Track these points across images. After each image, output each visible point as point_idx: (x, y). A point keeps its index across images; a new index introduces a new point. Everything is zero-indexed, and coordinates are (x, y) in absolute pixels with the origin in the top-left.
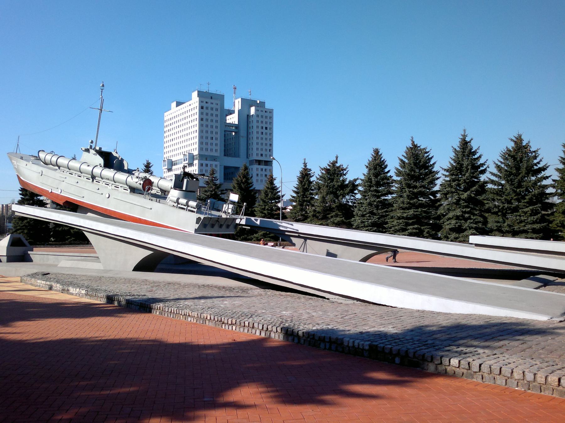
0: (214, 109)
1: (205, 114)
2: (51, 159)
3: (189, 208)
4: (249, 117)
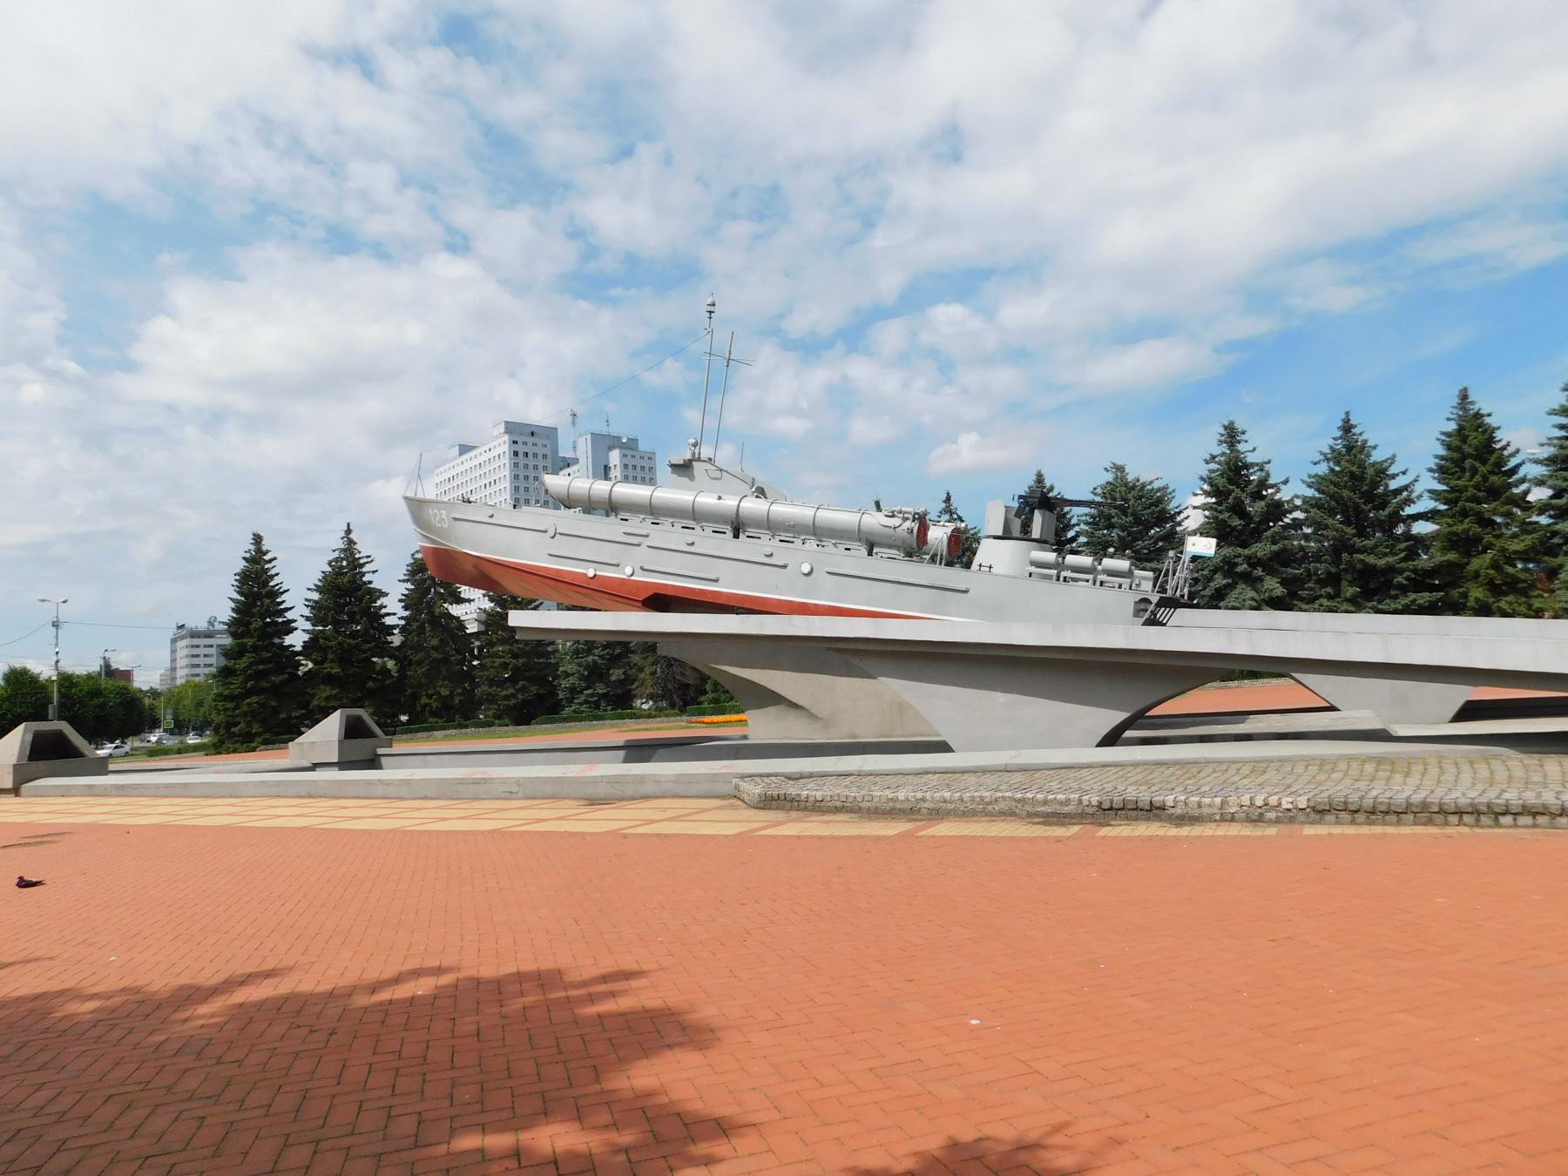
1: (521, 466)
3: (1064, 574)
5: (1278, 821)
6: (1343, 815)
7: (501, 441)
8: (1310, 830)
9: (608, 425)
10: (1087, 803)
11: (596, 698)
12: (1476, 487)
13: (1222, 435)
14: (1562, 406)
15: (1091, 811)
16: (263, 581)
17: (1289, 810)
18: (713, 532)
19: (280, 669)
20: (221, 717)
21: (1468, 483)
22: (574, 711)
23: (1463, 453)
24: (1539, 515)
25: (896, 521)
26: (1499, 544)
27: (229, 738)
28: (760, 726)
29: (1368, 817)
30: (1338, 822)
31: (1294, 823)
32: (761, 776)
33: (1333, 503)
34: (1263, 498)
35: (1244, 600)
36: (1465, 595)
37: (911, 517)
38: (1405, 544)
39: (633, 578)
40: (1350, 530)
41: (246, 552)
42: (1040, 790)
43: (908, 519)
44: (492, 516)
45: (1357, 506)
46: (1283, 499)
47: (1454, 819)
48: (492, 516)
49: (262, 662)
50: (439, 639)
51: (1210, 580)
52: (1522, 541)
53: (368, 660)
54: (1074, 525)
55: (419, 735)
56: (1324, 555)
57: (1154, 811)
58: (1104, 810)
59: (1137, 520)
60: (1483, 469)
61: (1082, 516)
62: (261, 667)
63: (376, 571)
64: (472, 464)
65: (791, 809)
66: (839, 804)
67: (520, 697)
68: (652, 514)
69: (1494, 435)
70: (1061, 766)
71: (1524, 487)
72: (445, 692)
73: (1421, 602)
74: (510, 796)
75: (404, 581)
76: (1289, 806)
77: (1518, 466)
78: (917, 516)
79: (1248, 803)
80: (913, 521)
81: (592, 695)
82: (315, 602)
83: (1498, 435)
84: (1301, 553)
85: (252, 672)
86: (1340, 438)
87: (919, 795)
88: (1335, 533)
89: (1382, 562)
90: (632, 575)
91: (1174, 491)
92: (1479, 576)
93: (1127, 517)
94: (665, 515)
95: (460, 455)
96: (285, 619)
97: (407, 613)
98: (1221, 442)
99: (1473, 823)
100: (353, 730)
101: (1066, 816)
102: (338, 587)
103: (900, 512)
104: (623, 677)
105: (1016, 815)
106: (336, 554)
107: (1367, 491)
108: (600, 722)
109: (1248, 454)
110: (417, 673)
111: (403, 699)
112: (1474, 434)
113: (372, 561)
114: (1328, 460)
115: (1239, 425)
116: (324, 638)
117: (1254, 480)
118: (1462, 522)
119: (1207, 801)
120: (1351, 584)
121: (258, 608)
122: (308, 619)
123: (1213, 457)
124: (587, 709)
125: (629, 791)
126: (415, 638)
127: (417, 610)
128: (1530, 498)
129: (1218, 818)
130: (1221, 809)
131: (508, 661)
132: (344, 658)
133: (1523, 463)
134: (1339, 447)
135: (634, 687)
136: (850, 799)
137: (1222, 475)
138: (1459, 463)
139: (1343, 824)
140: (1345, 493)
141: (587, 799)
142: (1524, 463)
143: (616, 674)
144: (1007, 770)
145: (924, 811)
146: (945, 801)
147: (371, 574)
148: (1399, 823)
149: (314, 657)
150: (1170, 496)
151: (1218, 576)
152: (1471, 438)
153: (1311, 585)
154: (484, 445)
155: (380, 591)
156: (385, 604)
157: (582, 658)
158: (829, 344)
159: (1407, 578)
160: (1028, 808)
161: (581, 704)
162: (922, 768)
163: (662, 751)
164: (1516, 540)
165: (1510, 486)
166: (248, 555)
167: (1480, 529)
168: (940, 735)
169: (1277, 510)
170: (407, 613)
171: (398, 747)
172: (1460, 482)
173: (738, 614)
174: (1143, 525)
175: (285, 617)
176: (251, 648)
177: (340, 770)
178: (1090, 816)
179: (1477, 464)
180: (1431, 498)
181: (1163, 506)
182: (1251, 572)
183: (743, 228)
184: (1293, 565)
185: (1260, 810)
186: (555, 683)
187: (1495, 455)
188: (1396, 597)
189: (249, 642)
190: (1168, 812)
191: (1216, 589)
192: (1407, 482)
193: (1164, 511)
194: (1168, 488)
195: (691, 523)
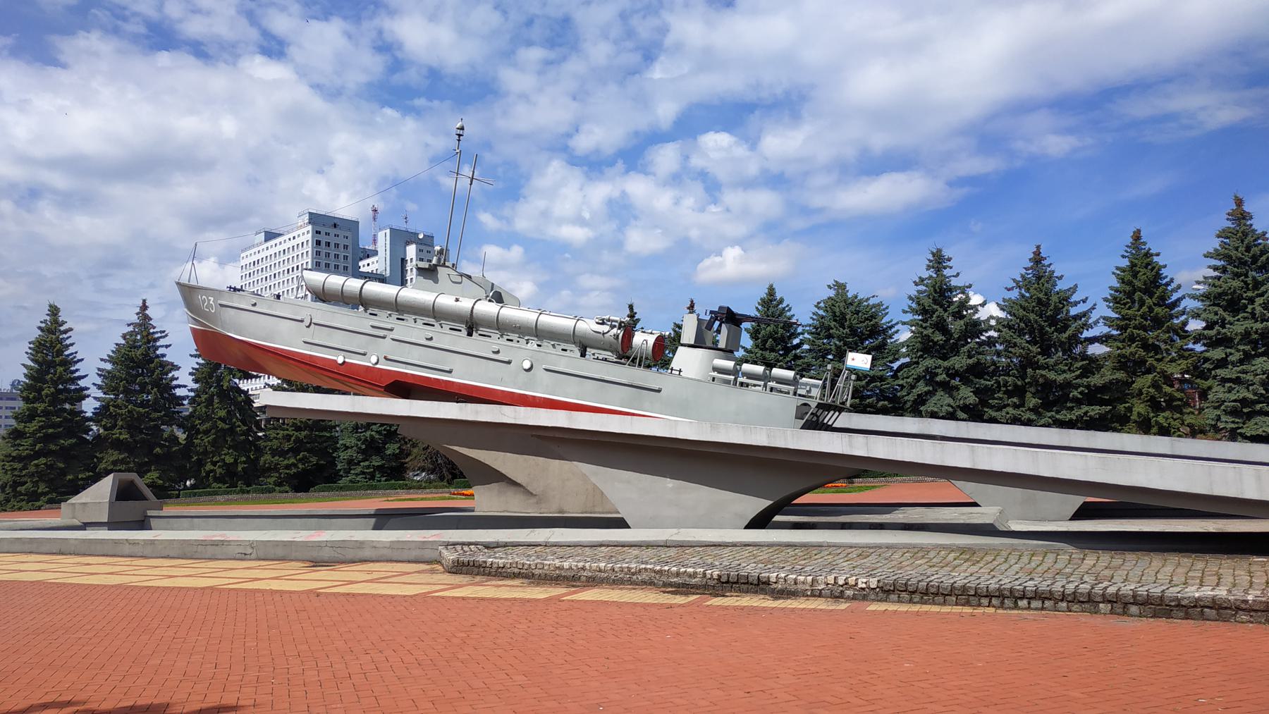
0: (341, 247)
1: (323, 254)
3: (741, 379)
5: (854, 598)
6: (904, 595)
7: (305, 230)
8: (874, 607)
9: (406, 222)
10: (710, 576)
11: (372, 470)
12: (1143, 317)
13: (930, 261)
14: (1216, 250)
15: (711, 583)
16: (58, 350)
17: (863, 589)
18: (451, 329)
19: (70, 433)
20: (7, 477)
21: (1136, 313)
22: (351, 481)
23: (1133, 286)
24: (1194, 343)
25: (605, 328)
26: (1160, 366)
27: (15, 497)
28: (485, 500)
29: (922, 598)
30: (900, 601)
31: (867, 600)
32: (463, 544)
33: (1022, 325)
34: (962, 317)
35: (942, 406)
36: (1130, 409)
37: (617, 324)
38: (1081, 364)
39: (378, 366)
40: (1035, 349)
41: (41, 322)
42: (792, 571)
43: (615, 326)
44: (254, 305)
45: (1042, 328)
46: (982, 319)
47: (985, 601)
48: (254, 305)
49: (53, 426)
50: (226, 410)
51: (913, 387)
52: (1179, 365)
53: (157, 427)
54: (799, 334)
55: (202, 499)
56: (1012, 369)
57: (760, 586)
58: (723, 583)
59: (853, 332)
60: (1149, 301)
61: (806, 326)
62: (51, 431)
63: (170, 345)
64: (276, 250)
65: (478, 574)
66: (516, 570)
67: (300, 466)
68: (397, 311)
69: (1161, 272)
70: (707, 544)
71: (1183, 318)
72: (229, 460)
73: (1092, 413)
74: (244, 557)
75: (195, 356)
76: (864, 586)
77: (1179, 300)
78: (623, 325)
79: (833, 582)
80: (619, 328)
81: (368, 467)
82: (109, 372)
83: (1164, 272)
84: (993, 367)
85: (42, 435)
86: (1031, 268)
87: (580, 565)
88: (1022, 351)
89: (1060, 378)
90: (377, 363)
91: (887, 308)
92: (1142, 394)
93: (844, 329)
94: (408, 313)
95: (266, 240)
96: (78, 387)
97: (196, 386)
98: (929, 268)
99: (999, 605)
100: (125, 493)
101: (693, 586)
102: (132, 360)
103: (609, 320)
104: (398, 451)
105: (654, 584)
106: (131, 328)
107: (1051, 316)
108: (374, 492)
109: (952, 278)
110: (203, 442)
111: (188, 465)
112: (1143, 271)
113: (166, 335)
114: (1020, 288)
115: (946, 253)
116: (114, 406)
117: (956, 301)
118: (1130, 346)
119: (801, 578)
120: (1034, 395)
121: (51, 375)
122: (99, 387)
123: (922, 280)
124: (363, 480)
125: (350, 554)
126: (204, 409)
127: (207, 383)
128: (1188, 328)
129: (809, 593)
130: (811, 586)
131: (291, 433)
132: (133, 425)
133: (1183, 297)
134: (1029, 276)
135: (407, 460)
136: (526, 567)
137: (928, 296)
138: (1130, 295)
139: (904, 602)
140: (1032, 316)
141: (313, 562)
142: (1185, 298)
143: (392, 448)
144: (666, 545)
145: (583, 579)
146: (600, 571)
147: (164, 349)
148: (944, 603)
149: (103, 423)
150: (883, 312)
151: (921, 384)
152: (1141, 274)
153: (1000, 395)
154: (288, 233)
155: (172, 364)
156: (176, 376)
157: (361, 433)
158: (611, 162)
159: (1081, 393)
160: (664, 579)
161: (357, 475)
162: (598, 542)
163: (392, 520)
164: (1174, 364)
165: (1171, 317)
166: (43, 325)
167: (1144, 353)
168: (619, 513)
169: (975, 328)
170: (196, 386)
171: (169, 510)
172: (1130, 312)
173: (457, 402)
174: (858, 336)
175: (79, 385)
176: (41, 412)
177: (109, 530)
178: (712, 588)
179: (1145, 297)
180: (1105, 324)
181: (876, 320)
182: (949, 382)
183: (535, 54)
184: (986, 377)
185: (841, 588)
186: (334, 455)
187: (1161, 289)
188: (1071, 409)
189: (40, 407)
190: (772, 587)
191: (918, 395)
192: (1085, 309)
193: (876, 325)
194: (882, 305)
195: (432, 321)
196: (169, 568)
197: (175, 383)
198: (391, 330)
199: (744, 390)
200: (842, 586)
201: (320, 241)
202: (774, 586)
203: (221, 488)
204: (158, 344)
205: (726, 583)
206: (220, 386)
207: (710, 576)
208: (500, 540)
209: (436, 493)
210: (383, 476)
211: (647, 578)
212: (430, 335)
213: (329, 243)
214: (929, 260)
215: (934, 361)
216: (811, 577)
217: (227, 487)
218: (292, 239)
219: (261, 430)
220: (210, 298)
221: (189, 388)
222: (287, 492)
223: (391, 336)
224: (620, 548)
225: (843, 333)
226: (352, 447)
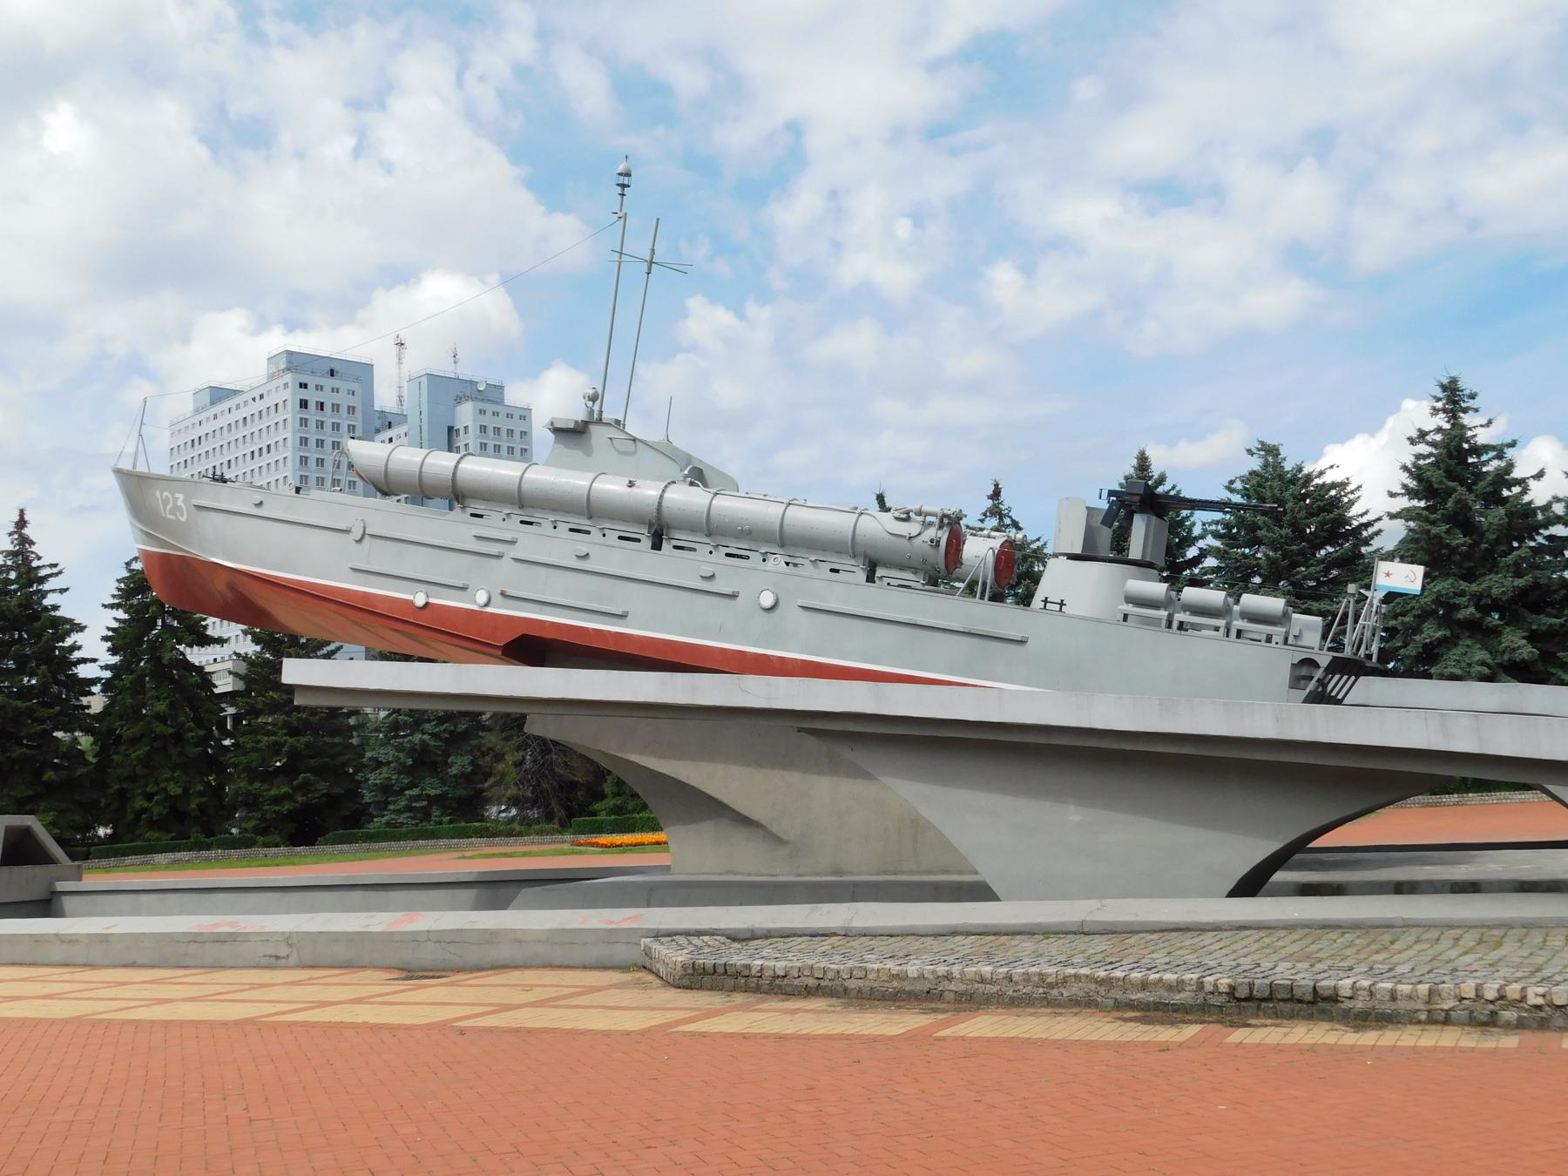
0: (344, 410)
2: (389, 456)
4: (455, 432)
5: (1520, 1025)
11: (425, 803)
17: (1538, 1007)
18: (620, 538)
22: (388, 824)
25: (912, 528)
31: (1548, 1028)
35: (1470, 665)
39: (489, 610)
43: (931, 524)
50: (167, 701)
51: (1417, 630)
53: (47, 735)
54: (1197, 539)
55: (129, 860)
58: (1239, 1000)
64: (231, 418)
65: (734, 990)
66: (811, 982)
68: (521, 507)
70: (1164, 927)
72: (175, 790)
74: (274, 962)
75: (112, 606)
76: (1540, 1001)
79: (1472, 994)
80: (941, 527)
81: (418, 798)
90: (486, 605)
93: (1281, 527)
95: (212, 403)
97: (115, 660)
98: (1435, 411)
101: (1177, 1008)
103: (919, 513)
108: (431, 842)
113: (60, 572)
115: (1466, 385)
119: (1405, 988)
123: (1423, 434)
125: (473, 955)
126: (129, 701)
129: (1423, 1017)
130: (1428, 1002)
135: (487, 785)
136: (830, 975)
141: (402, 969)
143: (459, 764)
144: (1083, 931)
146: (983, 981)
161: (399, 812)
163: (527, 892)
170: (115, 660)
171: (94, 879)
182: (1481, 619)
185: (1491, 1007)
195: (583, 523)
196: (149, 986)
197: (76, 655)
198: (513, 542)
199: (1175, 637)
200: (1492, 1002)
201: (306, 402)
202: (1348, 1004)
203: (161, 840)
204: (46, 587)
205: (1245, 1000)
206: (156, 659)
207: (1212, 988)
208: (757, 926)
209: (542, 844)
210: (443, 814)
211: (1081, 994)
212: (583, 550)
213: (322, 404)
214: (1435, 397)
215: (1452, 584)
216: (1427, 986)
217: (172, 839)
218: (258, 398)
219: (228, 734)
220: (177, 495)
221: (103, 664)
222: (277, 845)
223: (513, 554)
224: (991, 938)
225: (1280, 535)
226: (389, 763)
